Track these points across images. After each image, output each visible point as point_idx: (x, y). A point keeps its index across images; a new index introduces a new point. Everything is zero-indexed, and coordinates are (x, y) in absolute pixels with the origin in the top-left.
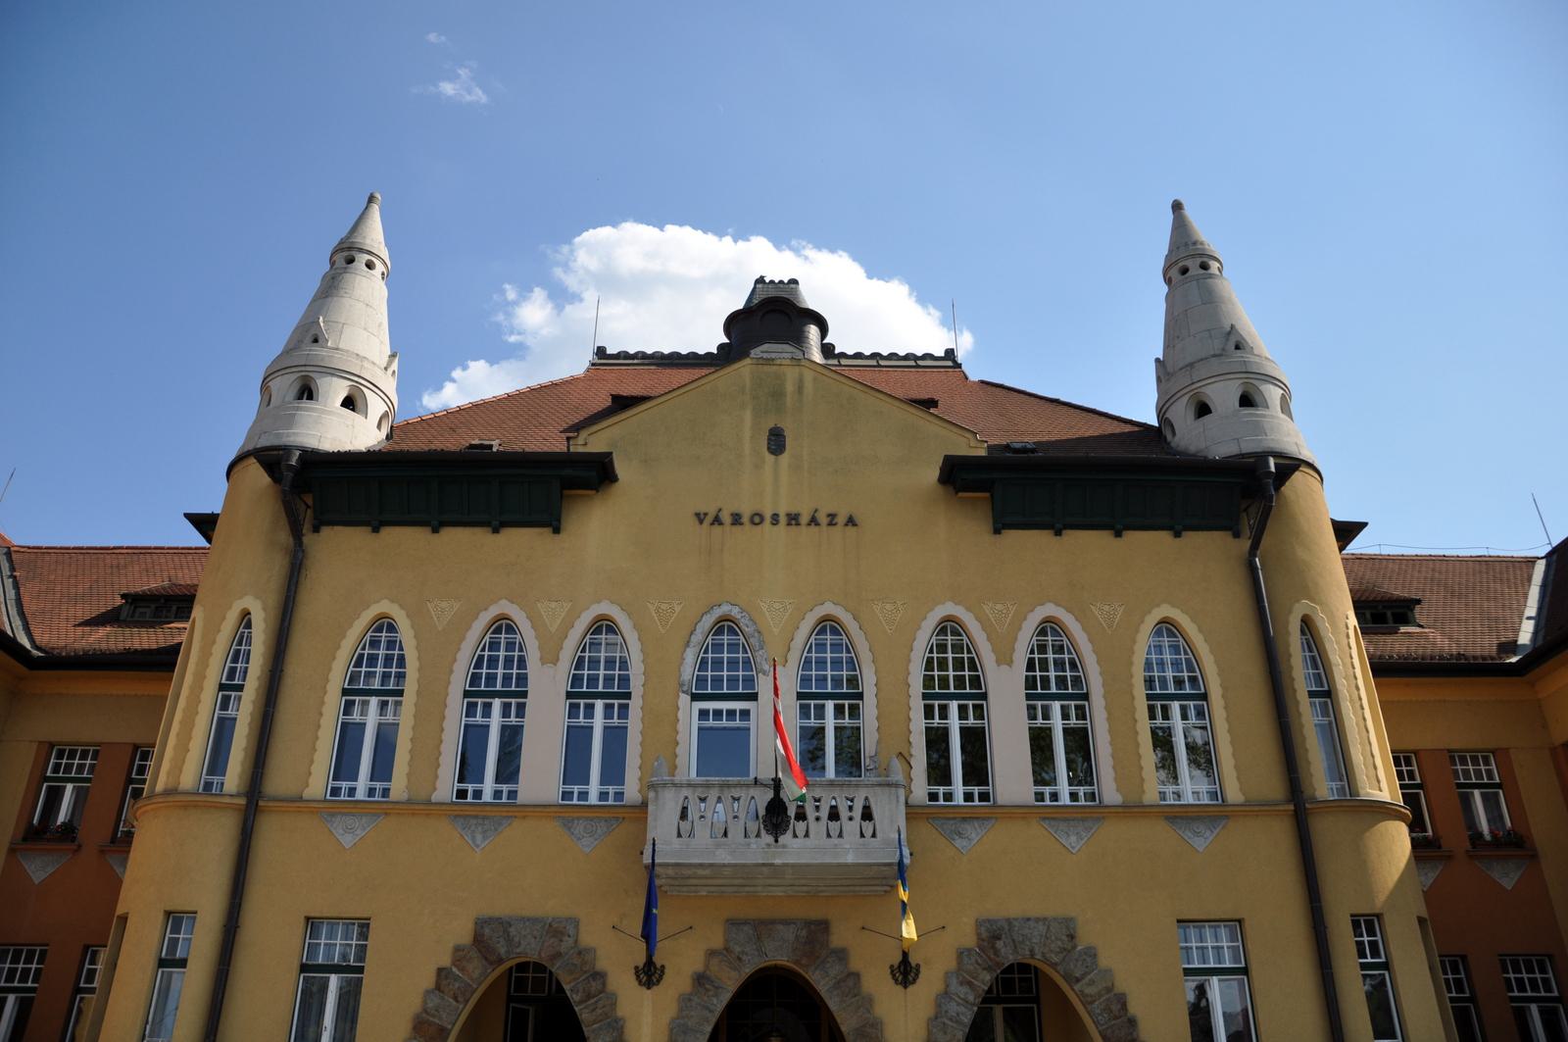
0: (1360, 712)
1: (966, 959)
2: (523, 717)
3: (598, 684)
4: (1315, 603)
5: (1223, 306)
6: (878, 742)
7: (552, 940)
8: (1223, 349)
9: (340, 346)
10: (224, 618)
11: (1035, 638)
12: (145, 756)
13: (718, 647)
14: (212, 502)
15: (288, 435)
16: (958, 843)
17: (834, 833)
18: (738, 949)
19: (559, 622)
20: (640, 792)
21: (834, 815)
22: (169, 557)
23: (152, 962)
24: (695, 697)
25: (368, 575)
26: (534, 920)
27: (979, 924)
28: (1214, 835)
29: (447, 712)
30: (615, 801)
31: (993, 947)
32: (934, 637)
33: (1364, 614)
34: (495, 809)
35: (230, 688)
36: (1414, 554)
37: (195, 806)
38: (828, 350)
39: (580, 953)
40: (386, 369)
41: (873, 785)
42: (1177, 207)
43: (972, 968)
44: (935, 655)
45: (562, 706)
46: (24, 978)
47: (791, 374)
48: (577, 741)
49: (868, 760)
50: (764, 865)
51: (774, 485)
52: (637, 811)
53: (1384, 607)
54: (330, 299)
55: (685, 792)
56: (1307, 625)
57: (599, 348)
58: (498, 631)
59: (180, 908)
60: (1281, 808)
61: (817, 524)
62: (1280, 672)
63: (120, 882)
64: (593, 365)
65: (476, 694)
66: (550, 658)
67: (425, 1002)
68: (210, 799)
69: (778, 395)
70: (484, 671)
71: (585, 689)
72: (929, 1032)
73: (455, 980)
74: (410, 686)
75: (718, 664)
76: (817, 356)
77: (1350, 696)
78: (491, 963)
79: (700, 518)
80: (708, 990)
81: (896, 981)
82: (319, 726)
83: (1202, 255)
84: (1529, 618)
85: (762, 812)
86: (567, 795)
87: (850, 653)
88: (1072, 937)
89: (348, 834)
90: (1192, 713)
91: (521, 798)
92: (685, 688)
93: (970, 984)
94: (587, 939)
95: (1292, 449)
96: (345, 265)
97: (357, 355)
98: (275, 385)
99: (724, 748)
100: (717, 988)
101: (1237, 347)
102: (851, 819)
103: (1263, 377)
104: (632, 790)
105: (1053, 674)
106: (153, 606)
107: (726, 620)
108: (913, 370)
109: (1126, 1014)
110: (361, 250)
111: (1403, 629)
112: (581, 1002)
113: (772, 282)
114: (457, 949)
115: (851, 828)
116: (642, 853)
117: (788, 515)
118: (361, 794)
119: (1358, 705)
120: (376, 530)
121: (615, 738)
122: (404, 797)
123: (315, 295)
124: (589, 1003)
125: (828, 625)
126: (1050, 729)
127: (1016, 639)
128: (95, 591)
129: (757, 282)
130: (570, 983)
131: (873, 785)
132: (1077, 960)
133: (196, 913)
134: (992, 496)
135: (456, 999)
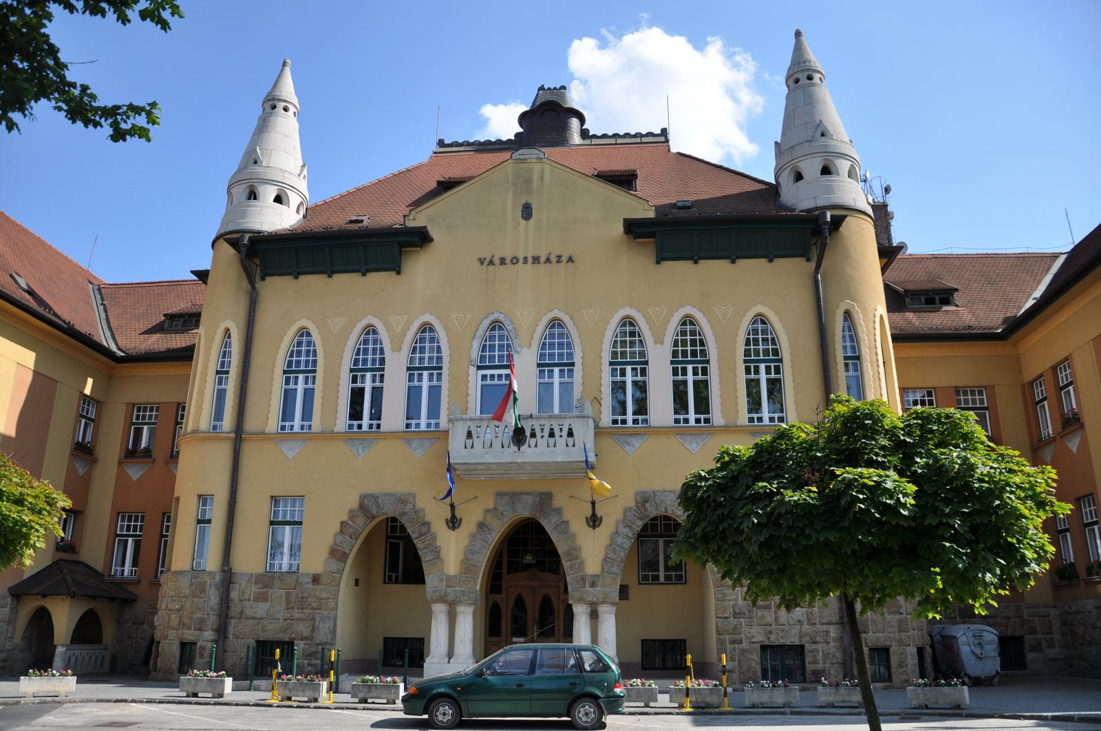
1: (628, 513)
2: (572, 377)
3: (426, 361)
4: (853, 301)
6: (583, 391)
8: (813, 137)
10: (216, 333)
12: (183, 409)
16: (627, 448)
17: (551, 444)
18: (501, 508)
21: (552, 435)
23: (194, 522)
24: (479, 368)
25: (295, 304)
26: (392, 495)
27: (636, 494)
29: (341, 382)
31: (644, 507)
35: (222, 373)
37: (209, 439)
38: (585, 134)
39: (416, 512)
40: (299, 175)
42: (798, 34)
45: (404, 375)
46: (135, 530)
47: (537, 168)
48: (413, 395)
50: (512, 463)
51: (526, 239)
53: (934, 294)
55: (469, 423)
56: (848, 315)
58: (368, 333)
59: (204, 493)
61: (550, 262)
63: (176, 476)
64: (435, 153)
65: (290, 372)
66: (397, 348)
67: (335, 539)
68: (216, 435)
69: (528, 182)
70: (361, 357)
72: (607, 553)
74: (320, 368)
75: (552, 345)
76: (576, 139)
79: (481, 261)
82: (271, 392)
85: (512, 434)
89: (290, 450)
90: (851, 367)
93: (630, 527)
94: (420, 504)
95: (849, 202)
96: (271, 111)
99: (500, 398)
101: (823, 135)
102: (561, 436)
104: (443, 422)
105: (690, 349)
106: (182, 320)
110: (280, 100)
111: (945, 308)
112: (417, 538)
113: (549, 89)
114: (351, 511)
115: (561, 441)
117: (533, 257)
118: (297, 429)
119: (875, 365)
120: (296, 278)
121: (435, 392)
125: (555, 323)
127: (666, 328)
128: (149, 312)
129: (539, 89)
131: (574, 417)
135: (351, 537)
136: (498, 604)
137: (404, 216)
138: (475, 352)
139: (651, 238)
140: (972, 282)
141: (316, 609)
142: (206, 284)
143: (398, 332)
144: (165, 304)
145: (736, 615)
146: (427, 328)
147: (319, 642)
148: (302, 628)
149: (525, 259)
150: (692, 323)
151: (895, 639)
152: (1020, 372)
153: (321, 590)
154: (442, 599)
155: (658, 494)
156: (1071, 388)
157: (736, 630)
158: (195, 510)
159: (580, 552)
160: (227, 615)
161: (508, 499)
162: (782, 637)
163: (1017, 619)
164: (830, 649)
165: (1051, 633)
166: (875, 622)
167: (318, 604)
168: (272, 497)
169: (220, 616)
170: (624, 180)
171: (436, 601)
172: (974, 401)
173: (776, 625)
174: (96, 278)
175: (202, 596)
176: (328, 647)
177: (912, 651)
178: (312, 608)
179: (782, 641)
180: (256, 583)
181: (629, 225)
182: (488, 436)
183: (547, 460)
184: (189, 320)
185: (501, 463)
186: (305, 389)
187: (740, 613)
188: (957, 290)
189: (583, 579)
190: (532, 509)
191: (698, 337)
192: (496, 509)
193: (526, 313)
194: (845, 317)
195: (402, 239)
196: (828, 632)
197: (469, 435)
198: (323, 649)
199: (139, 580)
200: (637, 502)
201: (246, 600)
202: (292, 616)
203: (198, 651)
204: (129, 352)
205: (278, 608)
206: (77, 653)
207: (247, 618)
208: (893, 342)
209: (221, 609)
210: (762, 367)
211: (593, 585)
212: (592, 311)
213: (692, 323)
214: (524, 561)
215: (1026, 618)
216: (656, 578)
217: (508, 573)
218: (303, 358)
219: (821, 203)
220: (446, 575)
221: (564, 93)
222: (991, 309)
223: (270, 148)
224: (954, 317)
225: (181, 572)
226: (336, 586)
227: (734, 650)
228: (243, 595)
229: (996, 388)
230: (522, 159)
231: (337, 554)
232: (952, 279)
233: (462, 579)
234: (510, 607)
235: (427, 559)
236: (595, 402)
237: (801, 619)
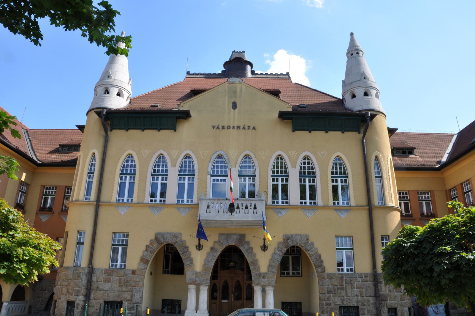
0: (389, 182)
1: (280, 245)
3: (187, 171)
4: (379, 152)
5: (362, 65)
7: (175, 239)
8: (360, 79)
9: (116, 78)
10: (88, 155)
11: (302, 161)
13: (218, 162)
14: (83, 122)
15: (103, 104)
16: (280, 215)
17: (246, 212)
18: (222, 241)
19: (176, 156)
20: (197, 200)
21: (247, 208)
22: (70, 132)
23: (75, 243)
24: (212, 176)
25: (128, 144)
27: (284, 236)
28: (347, 214)
30: (191, 203)
31: (287, 242)
32: (275, 160)
33: (400, 151)
34: (160, 205)
35: (91, 173)
36: (419, 132)
37: (84, 204)
38: (253, 72)
39: (182, 242)
40: (128, 84)
41: (257, 200)
42: (352, 34)
43: (281, 247)
44: (275, 165)
45: (177, 178)
47: (239, 86)
48: (181, 187)
49: (256, 193)
50: (228, 220)
52: (196, 206)
53: (406, 150)
54: (112, 64)
56: (377, 158)
57: (188, 72)
60: (365, 207)
61: (245, 129)
62: (368, 171)
63: (66, 223)
64: (186, 77)
65: (123, 174)
66: (174, 165)
67: (143, 254)
68: (87, 202)
69: (235, 92)
71: (183, 174)
72: (270, 263)
73: (150, 248)
74: (137, 173)
76: (249, 74)
77: (387, 178)
78: (159, 244)
79: (213, 127)
80: (214, 251)
81: (262, 250)
83: (357, 50)
84: (447, 153)
85: (228, 207)
86: (178, 201)
87: (253, 164)
88: (308, 240)
89: (123, 211)
91: (166, 202)
92: (209, 174)
94: (184, 238)
95: (377, 108)
97: (120, 81)
98: (98, 89)
100: (216, 251)
101: (364, 78)
102: (251, 209)
103: (371, 87)
104: (195, 200)
105: (307, 170)
107: (220, 155)
108: (276, 79)
109: (320, 259)
111: (411, 156)
112: (182, 254)
113: (237, 52)
114: (151, 241)
115: (251, 210)
116: (197, 217)
117: (237, 126)
118: (125, 201)
119: (389, 180)
121: (191, 186)
122: (137, 202)
123: (108, 63)
124: (184, 254)
126: (305, 185)
130: (179, 249)
131: (257, 200)
132: (309, 246)
134: (293, 122)
135: (151, 253)
136: (216, 285)
137: (178, 105)
138: (210, 169)
139: (290, 120)
141: (134, 286)
142: (83, 132)
143: (174, 158)
144: (59, 140)
145: (329, 292)
146: (188, 156)
147: (134, 302)
148: (127, 296)
150: (308, 159)
151: (399, 304)
152: (445, 185)
153: (136, 277)
154: (193, 283)
155: (293, 236)
156: (470, 193)
157: (328, 299)
158: (76, 238)
161: (225, 237)
162: (349, 302)
164: (370, 308)
166: (390, 296)
167: (134, 284)
169: (87, 289)
170: (276, 93)
172: (425, 197)
173: (346, 297)
174: (25, 126)
175: (78, 279)
176: (139, 304)
177: (406, 309)
178: (132, 286)
179: (349, 304)
181: (282, 114)
182: (217, 208)
187: (330, 291)
189: (259, 275)
190: (236, 241)
195: (178, 115)
196: (369, 300)
198: (137, 306)
200: (284, 239)
201: (99, 281)
202: (122, 289)
203: (76, 306)
204: (43, 161)
205: (115, 286)
206: (13, 305)
207: (100, 290)
208: (395, 170)
209: (87, 285)
210: (280, 179)
211: (264, 277)
212: (263, 152)
213: (308, 159)
216: (288, 273)
217: (220, 270)
218: (129, 168)
219: (364, 108)
220: (196, 272)
221: (244, 54)
222: (430, 157)
223: (116, 71)
225: (68, 267)
227: (328, 308)
228: (98, 279)
229: (435, 191)
230: (233, 82)
231: (143, 260)
232: (411, 143)
235: (187, 264)
236: (265, 193)
237: (358, 294)
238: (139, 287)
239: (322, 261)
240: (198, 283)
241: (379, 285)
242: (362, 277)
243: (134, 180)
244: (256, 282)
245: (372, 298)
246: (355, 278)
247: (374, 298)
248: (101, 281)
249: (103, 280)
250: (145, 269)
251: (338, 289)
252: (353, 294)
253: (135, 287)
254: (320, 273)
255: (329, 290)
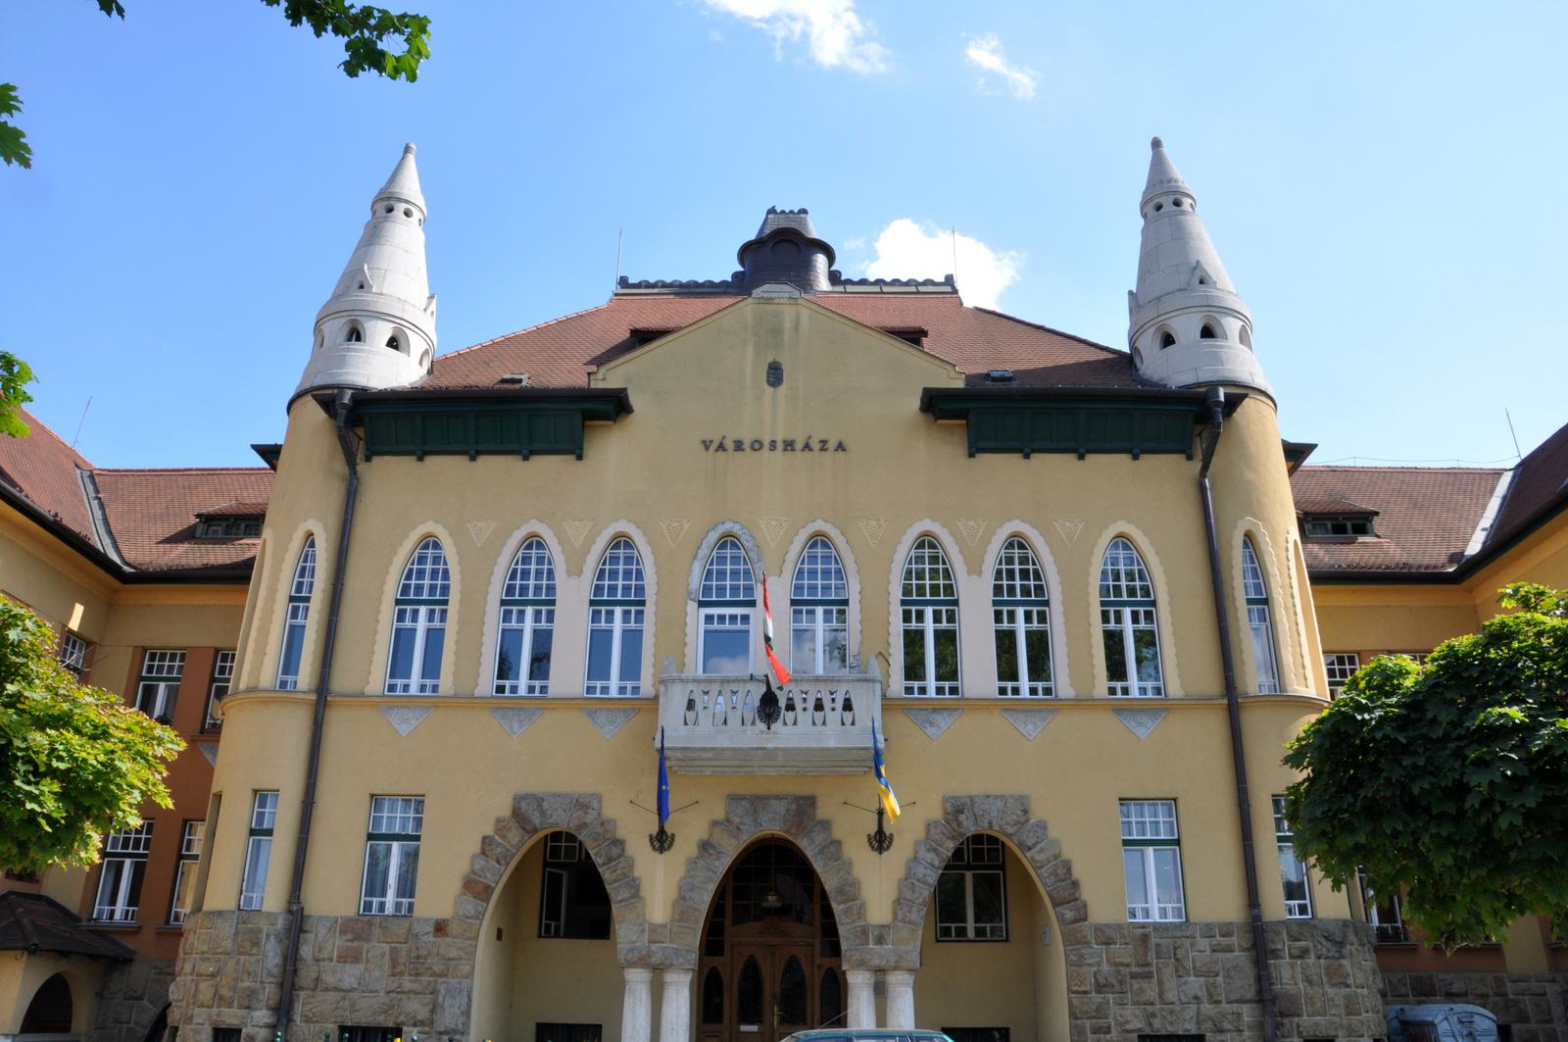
1: (933, 830)
3: (618, 588)
7: (579, 813)
8: (1188, 284)
16: (930, 730)
17: (819, 721)
21: (819, 706)
24: (702, 604)
25: (425, 501)
26: (565, 796)
27: (945, 800)
31: (957, 820)
35: (298, 600)
37: (274, 701)
38: (834, 277)
39: (602, 824)
40: (425, 310)
42: (1156, 144)
45: (586, 612)
46: (136, 846)
47: (788, 312)
48: (599, 643)
50: (758, 749)
51: (772, 414)
53: (1344, 519)
55: (691, 686)
56: (1249, 539)
64: (616, 295)
65: (405, 602)
66: (575, 571)
67: (472, 864)
68: (285, 695)
69: (776, 331)
72: (900, 891)
74: (454, 597)
75: (813, 573)
76: (823, 284)
79: (706, 445)
85: (757, 703)
89: (405, 724)
93: (935, 851)
94: (609, 812)
101: (1201, 282)
102: (833, 709)
104: (646, 685)
105: (1020, 581)
110: (400, 200)
111: (1361, 539)
112: (604, 864)
113: (783, 212)
114: (499, 821)
115: (834, 716)
117: (784, 442)
118: (414, 690)
121: (633, 639)
131: (853, 681)
133: (278, 791)
135: (498, 862)
136: (718, 972)
138: (696, 580)
140: (1392, 506)
143: (577, 545)
145: (1100, 988)
146: (621, 542)
147: (442, 1029)
148: (417, 1007)
149: (773, 445)
154: (642, 962)
157: (1100, 1011)
159: (859, 889)
160: (293, 985)
162: (1171, 1023)
163: (1497, 998)
165: (1550, 1021)
166: (1311, 999)
168: (372, 796)
169: (281, 985)
170: (913, 336)
171: (632, 965)
173: (1161, 1003)
175: (254, 951)
178: (434, 974)
179: (1171, 1029)
180: (343, 932)
183: (813, 744)
184: (249, 522)
185: (740, 749)
186: (429, 630)
187: (1105, 986)
188: (1377, 514)
189: (865, 931)
191: (1031, 567)
192: (728, 820)
193: (774, 523)
194: (1245, 542)
195: (588, 406)
196: (1239, 1015)
197: (691, 705)
199: (139, 928)
200: (946, 813)
201: (324, 960)
202: (400, 986)
205: (377, 974)
207: (326, 989)
211: (880, 940)
212: (873, 523)
213: (1021, 546)
214: (765, 904)
215: (1511, 996)
216: (962, 932)
218: (427, 582)
219: (1206, 375)
220: (651, 924)
224: (1376, 551)
225: (220, 913)
226: (472, 939)
228: (320, 951)
230: (767, 299)
231: (474, 887)
233: (675, 929)
234: (736, 978)
235: (620, 898)
237: (1200, 994)
238: (457, 977)
239: (1075, 884)
240: (659, 962)
241: (1269, 961)
242: (1214, 937)
243: (443, 619)
244: (854, 958)
245: (1248, 1005)
246: (1188, 941)
247: (1254, 1005)
248: (331, 960)
249: (335, 956)
250: (479, 916)
251: (1134, 976)
252: (1182, 994)
253: (444, 979)
254: (1069, 924)
255: (1102, 981)
